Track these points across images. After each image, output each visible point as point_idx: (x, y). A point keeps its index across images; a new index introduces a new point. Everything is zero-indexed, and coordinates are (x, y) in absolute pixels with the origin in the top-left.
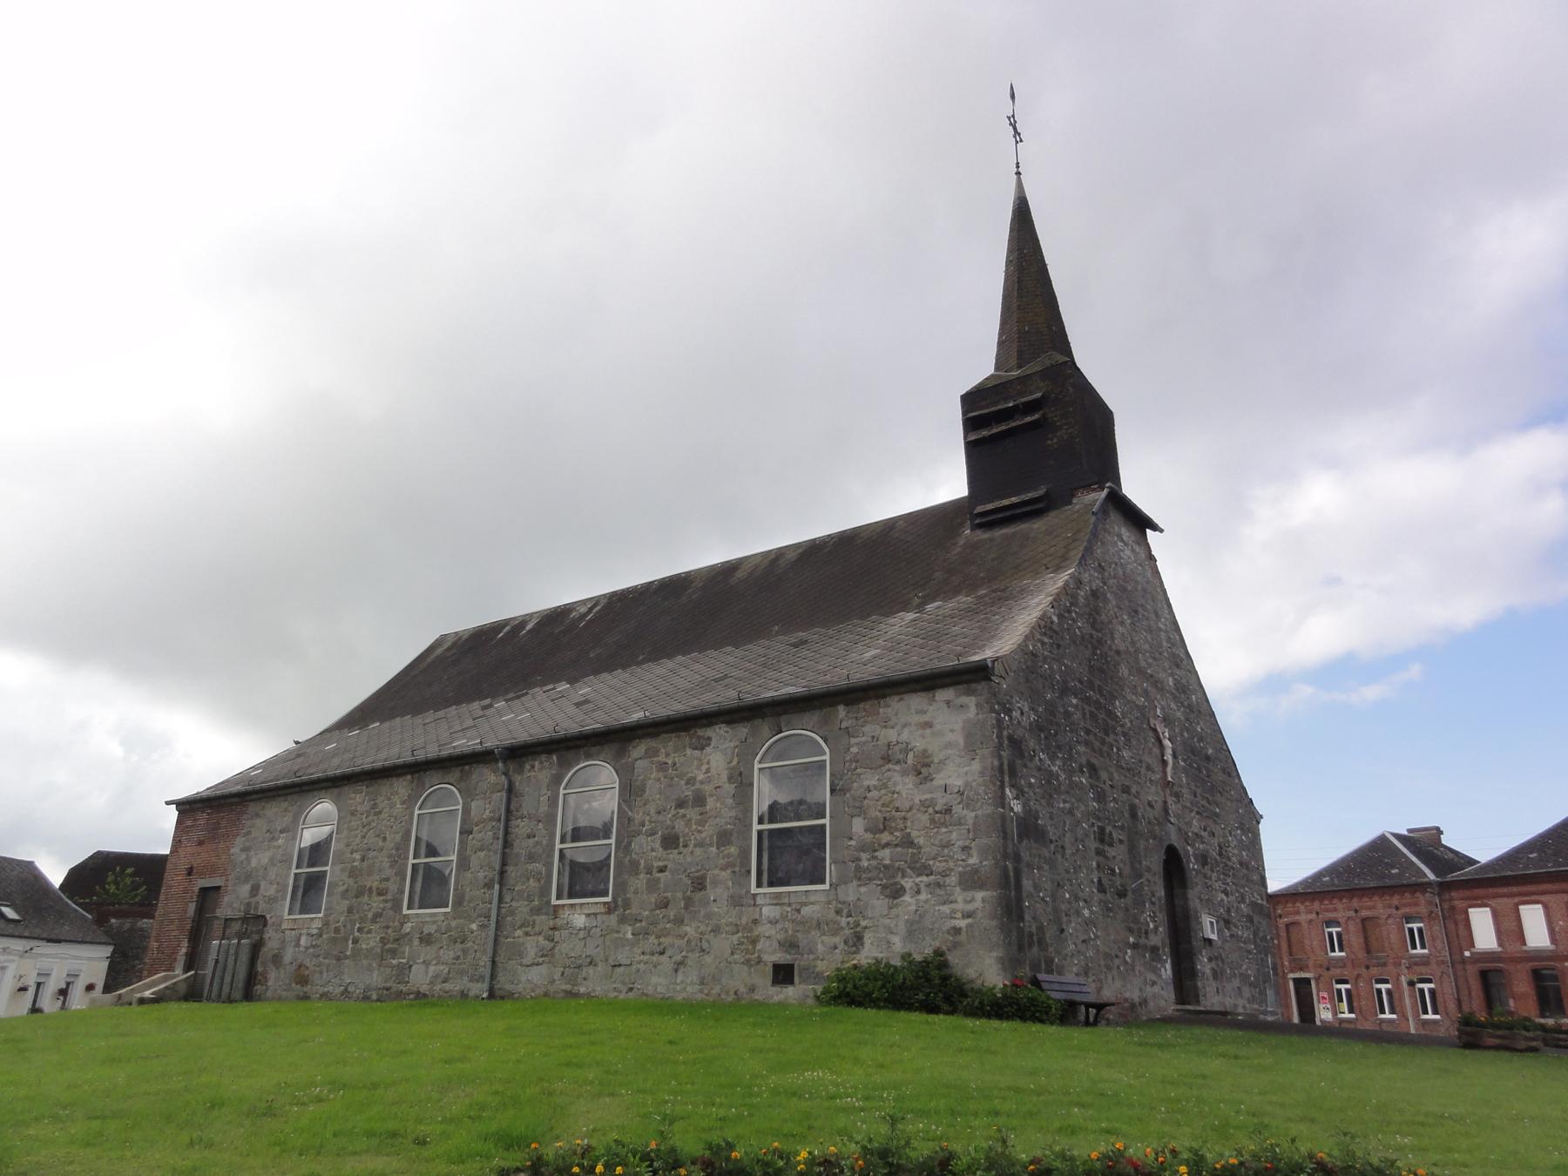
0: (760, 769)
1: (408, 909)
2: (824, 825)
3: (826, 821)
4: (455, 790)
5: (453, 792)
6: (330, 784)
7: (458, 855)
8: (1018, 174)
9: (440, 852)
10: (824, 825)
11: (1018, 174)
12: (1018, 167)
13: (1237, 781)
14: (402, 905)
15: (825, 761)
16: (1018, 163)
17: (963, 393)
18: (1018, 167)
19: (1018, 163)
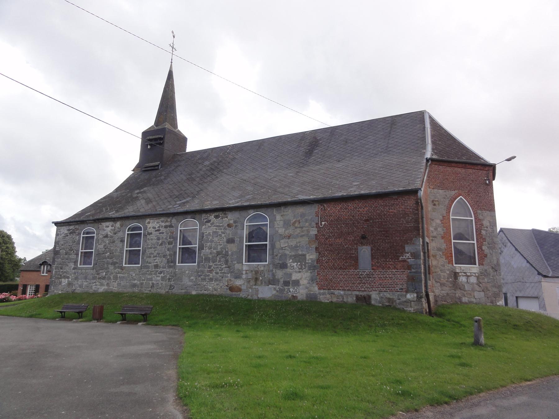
0: (246, 225)
1: (178, 263)
2: (267, 244)
3: (268, 243)
4: (197, 221)
5: (197, 224)
6: (93, 221)
7: (451, 242)
8: (171, 62)
9: (192, 243)
10: (267, 244)
11: (171, 62)
12: (172, 60)
13: (552, 235)
14: (176, 262)
15: (268, 224)
16: (172, 59)
17: (143, 132)
18: (172, 60)
19: (172, 59)
